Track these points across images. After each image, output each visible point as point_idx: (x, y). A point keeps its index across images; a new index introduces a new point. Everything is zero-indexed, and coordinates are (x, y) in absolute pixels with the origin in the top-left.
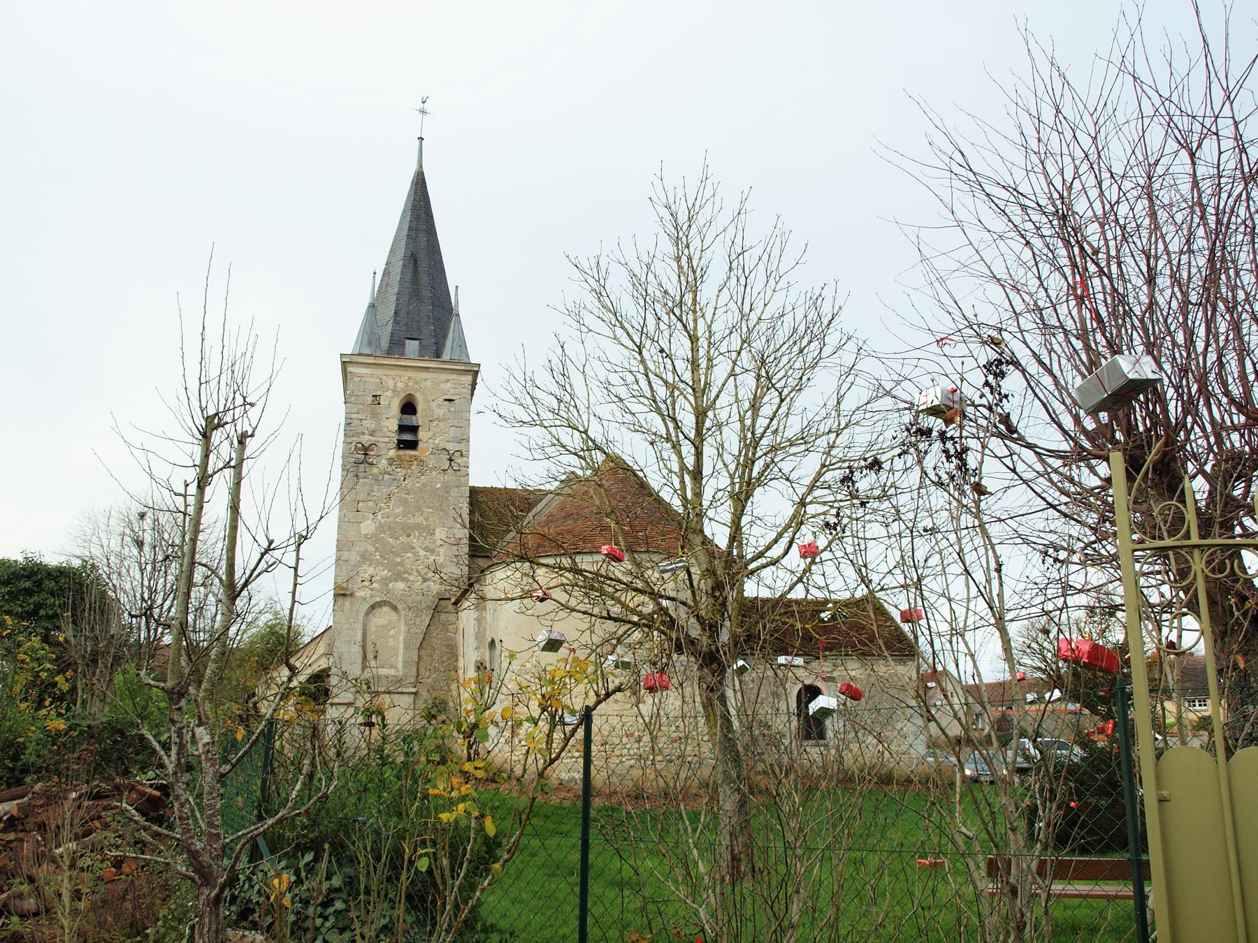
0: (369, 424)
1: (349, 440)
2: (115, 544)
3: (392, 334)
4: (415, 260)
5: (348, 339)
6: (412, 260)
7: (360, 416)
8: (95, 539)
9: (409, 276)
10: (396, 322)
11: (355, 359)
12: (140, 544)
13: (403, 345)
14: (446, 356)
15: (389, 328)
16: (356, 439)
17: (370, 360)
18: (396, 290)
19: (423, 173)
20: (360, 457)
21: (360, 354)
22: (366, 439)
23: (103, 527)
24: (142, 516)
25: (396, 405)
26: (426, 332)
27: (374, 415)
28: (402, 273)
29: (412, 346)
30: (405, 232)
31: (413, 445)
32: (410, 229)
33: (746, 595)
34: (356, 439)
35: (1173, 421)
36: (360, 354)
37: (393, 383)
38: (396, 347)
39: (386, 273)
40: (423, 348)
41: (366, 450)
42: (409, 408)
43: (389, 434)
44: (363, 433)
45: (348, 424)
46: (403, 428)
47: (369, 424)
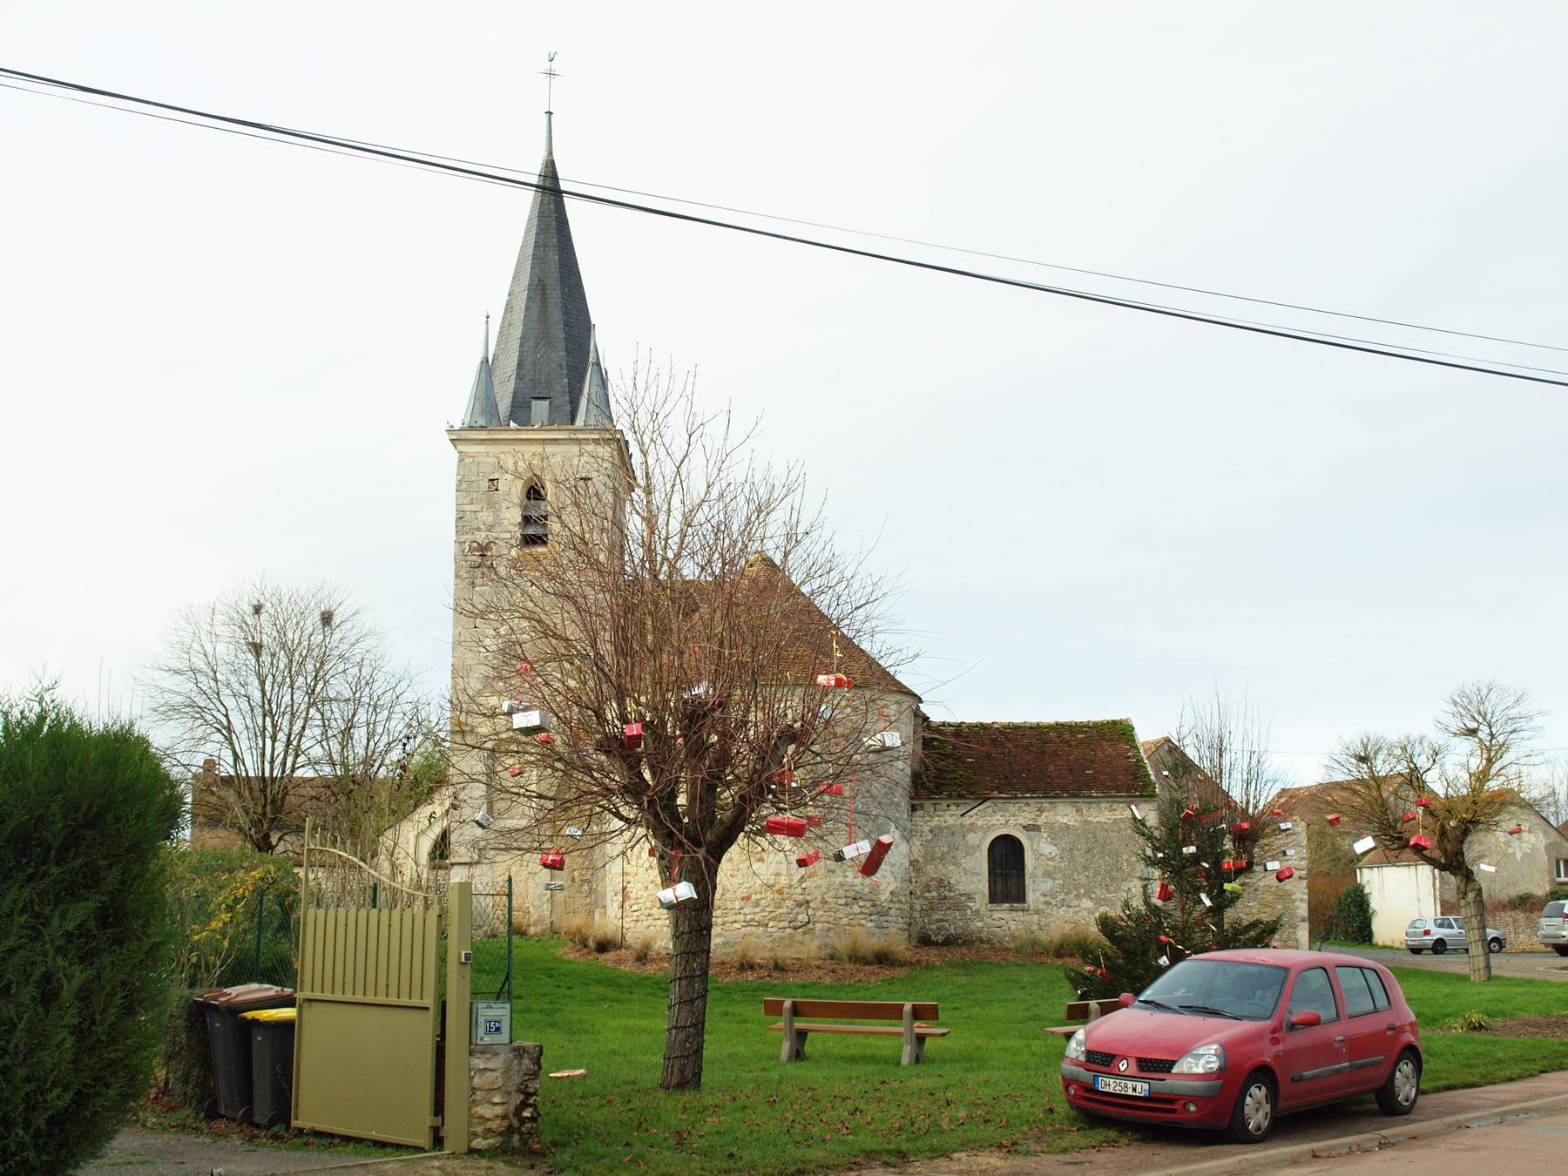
0: (487, 517)
1: (463, 538)
2: (223, 650)
3: (515, 393)
4: (544, 290)
5: (458, 406)
6: (538, 288)
7: (474, 508)
8: (196, 646)
9: (535, 312)
10: (519, 377)
11: (465, 435)
12: (257, 648)
13: (530, 407)
14: (579, 422)
15: (511, 386)
16: (469, 537)
17: (483, 435)
18: (519, 333)
19: (553, 163)
20: (478, 559)
21: (471, 428)
22: (481, 537)
23: (207, 627)
24: (257, 610)
25: (518, 489)
26: (558, 387)
27: (492, 505)
28: (527, 308)
29: (540, 408)
30: (530, 250)
31: (539, 540)
32: (537, 245)
33: (508, 1006)
34: (469, 537)
35: (491, 1141)
36: (471, 428)
37: (515, 457)
38: (520, 411)
39: (509, 308)
40: (553, 409)
41: (483, 550)
42: (534, 492)
43: (511, 528)
44: (479, 529)
45: (459, 519)
46: (527, 520)
47: (487, 517)
